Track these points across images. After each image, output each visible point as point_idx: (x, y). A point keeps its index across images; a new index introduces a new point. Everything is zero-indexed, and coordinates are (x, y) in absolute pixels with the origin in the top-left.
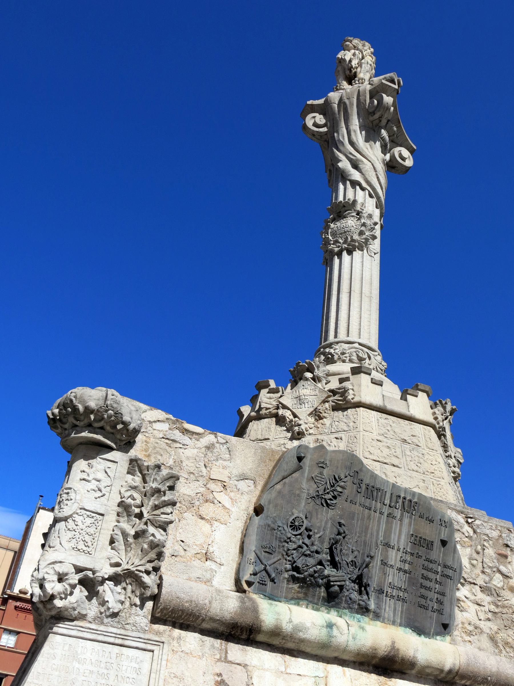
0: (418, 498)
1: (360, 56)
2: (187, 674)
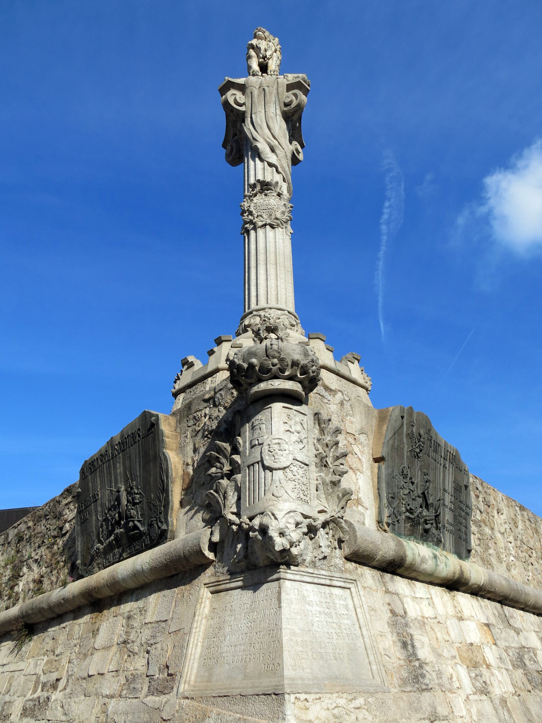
0: (456, 453)
1: (270, 46)
2: (376, 606)
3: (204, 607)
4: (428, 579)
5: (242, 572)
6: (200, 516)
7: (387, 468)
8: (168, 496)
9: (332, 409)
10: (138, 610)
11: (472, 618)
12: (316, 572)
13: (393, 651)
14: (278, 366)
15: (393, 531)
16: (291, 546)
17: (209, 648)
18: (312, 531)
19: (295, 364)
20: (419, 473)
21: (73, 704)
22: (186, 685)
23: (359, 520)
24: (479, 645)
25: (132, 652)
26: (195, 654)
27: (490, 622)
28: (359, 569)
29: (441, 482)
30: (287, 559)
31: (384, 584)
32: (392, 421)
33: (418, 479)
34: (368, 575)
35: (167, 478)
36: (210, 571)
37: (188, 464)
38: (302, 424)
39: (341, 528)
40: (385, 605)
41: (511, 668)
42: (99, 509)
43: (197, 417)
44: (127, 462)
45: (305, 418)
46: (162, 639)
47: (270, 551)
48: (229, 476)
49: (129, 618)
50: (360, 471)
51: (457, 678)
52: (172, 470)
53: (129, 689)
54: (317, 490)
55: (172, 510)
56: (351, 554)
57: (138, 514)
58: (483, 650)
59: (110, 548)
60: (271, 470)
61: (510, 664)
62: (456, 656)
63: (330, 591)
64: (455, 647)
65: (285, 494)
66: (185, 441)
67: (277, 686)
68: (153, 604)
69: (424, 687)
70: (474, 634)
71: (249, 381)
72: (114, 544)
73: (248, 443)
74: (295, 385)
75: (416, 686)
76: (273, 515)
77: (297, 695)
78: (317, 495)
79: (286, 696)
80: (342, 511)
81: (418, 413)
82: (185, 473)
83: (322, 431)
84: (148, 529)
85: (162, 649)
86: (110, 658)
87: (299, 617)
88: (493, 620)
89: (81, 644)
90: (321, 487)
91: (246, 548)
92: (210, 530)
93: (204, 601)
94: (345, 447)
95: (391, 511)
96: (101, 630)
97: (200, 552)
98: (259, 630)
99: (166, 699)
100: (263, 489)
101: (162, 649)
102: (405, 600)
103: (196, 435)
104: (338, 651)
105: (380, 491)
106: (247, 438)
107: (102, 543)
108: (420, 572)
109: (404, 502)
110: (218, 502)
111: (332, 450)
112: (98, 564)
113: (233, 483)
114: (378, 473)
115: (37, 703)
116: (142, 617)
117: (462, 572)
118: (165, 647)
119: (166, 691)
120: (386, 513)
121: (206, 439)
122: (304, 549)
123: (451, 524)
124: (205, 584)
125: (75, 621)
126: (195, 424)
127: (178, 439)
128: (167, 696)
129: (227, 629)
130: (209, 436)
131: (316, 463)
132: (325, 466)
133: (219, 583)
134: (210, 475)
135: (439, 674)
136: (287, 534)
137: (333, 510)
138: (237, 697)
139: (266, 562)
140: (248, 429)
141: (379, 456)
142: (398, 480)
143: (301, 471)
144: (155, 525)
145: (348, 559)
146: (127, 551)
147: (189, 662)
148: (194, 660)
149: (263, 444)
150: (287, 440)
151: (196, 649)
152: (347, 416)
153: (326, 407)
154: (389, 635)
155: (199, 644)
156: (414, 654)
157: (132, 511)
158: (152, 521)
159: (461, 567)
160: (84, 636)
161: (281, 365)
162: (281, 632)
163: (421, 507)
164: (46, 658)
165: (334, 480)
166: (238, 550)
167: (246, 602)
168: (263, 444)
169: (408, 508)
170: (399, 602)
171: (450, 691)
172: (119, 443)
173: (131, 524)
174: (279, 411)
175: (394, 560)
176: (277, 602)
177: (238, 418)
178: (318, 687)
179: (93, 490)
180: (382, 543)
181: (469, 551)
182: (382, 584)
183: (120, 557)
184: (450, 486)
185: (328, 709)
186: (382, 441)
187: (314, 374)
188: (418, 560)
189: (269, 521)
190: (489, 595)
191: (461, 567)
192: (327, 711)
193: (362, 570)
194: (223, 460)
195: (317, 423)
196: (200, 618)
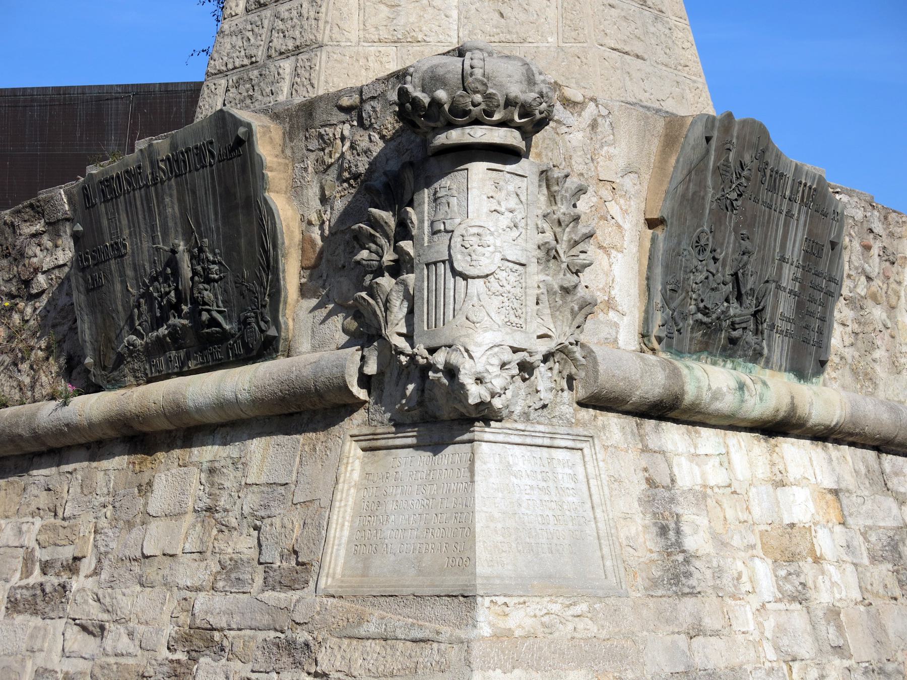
0: (818, 184)
2: (623, 475)
3: (352, 470)
4: (726, 423)
5: (413, 425)
6: (338, 321)
7: (668, 238)
8: (278, 280)
9: (575, 143)
10: (229, 461)
11: (805, 481)
12: (529, 428)
13: (641, 540)
14: (483, 106)
15: (669, 348)
16: (493, 397)
17: (362, 530)
18: (526, 368)
19: (509, 103)
20: (733, 237)
21: (120, 597)
22: (330, 580)
23: (608, 336)
24: (807, 526)
25: (227, 526)
26: (340, 538)
27: (843, 486)
28: (600, 418)
29: (778, 245)
30: (486, 414)
31: (642, 438)
32: (688, 149)
33: (728, 250)
34: (614, 425)
35: (275, 246)
36: (360, 416)
37: (310, 223)
38: (518, 195)
39: (574, 360)
40: (638, 471)
41: (866, 561)
42: (130, 273)
43: (326, 137)
44: (188, 199)
45: (523, 183)
46: (282, 511)
47: (460, 401)
48: (396, 270)
49: (212, 471)
50: (617, 250)
51: (750, 578)
52: (282, 233)
53: (228, 579)
54: (537, 303)
55: (285, 303)
56: (587, 398)
57: (217, 298)
58: (813, 533)
59: (160, 347)
60: (465, 277)
61: (865, 554)
62: (755, 545)
63: (550, 455)
64: (757, 531)
65: (486, 318)
66: (303, 178)
67: (467, 586)
68: (258, 456)
69: (687, 590)
70: (800, 506)
71: (432, 124)
72: (167, 343)
73: (426, 224)
74: (509, 134)
75: (674, 588)
76: (467, 351)
77: (494, 598)
78: (538, 310)
79: (479, 599)
80: (578, 331)
81: (744, 123)
82: (306, 241)
83: (552, 198)
84: (240, 329)
85: (283, 526)
86: (183, 531)
87: (500, 495)
88: (849, 481)
89: (117, 505)
90: (544, 298)
91: (421, 390)
92: (360, 353)
93: (351, 461)
94: (593, 209)
95: (668, 315)
96: (155, 487)
97: (344, 388)
98: (440, 511)
99: (298, 597)
100: (452, 307)
101: (283, 526)
102: (675, 461)
103: (325, 171)
104: (555, 541)
105: (651, 282)
106: (426, 214)
107: (141, 336)
108: (709, 414)
109: (694, 296)
110: (375, 313)
111: (568, 230)
112: (134, 371)
113: (401, 288)
114: (650, 250)
115: (39, 592)
116: (239, 474)
117: (793, 407)
118: (287, 525)
119: (296, 586)
120: (658, 318)
121: (345, 185)
122: (513, 397)
123: (788, 320)
124: (351, 436)
125: (95, 464)
126: (323, 150)
127: (290, 171)
128: (298, 592)
129: (391, 506)
130: (352, 181)
131: (538, 259)
132: (555, 258)
133: (375, 437)
134: (358, 263)
135: (718, 573)
136: (487, 381)
137: (561, 334)
138: (408, 598)
139: (453, 415)
140: (426, 200)
141: (655, 215)
142: (688, 257)
143: (513, 278)
144: (254, 325)
145: (582, 404)
146: (195, 358)
147: (333, 548)
148: (339, 545)
149: (453, 231)
150: (492, 229)
151: (342, 530)
152: (602, 147)
153: (564, 141)
154: (638, 518)
155: (346, 524)
156: (678, 544)
157: (205, 293)
158: (247, 317)
159: (792, 398)
160: (122, 492)
161: (487, 105)
162: (473, 517)
163: (727, 300)
164: (38, 522)
165: (566, 284)
166: (408, 393)
167: (421, 469)
168: (453, 231)
169: (701, 305)
170: (663, 466)
171: (733, 597)
172: (168, 158)
173: (205, 316)
174: (481, 176)
175: (661, 401)
176: (468, 474)
177: (409, 175)
178: (522, 589)
179: (111, 234)
180: (641, 377)
181: (823, 363)
182: (638, 439)
183: (181, 368)
184: (796, 249)
185: (535, 616)
186: (665, 187)
187: (543, 115)
188: (706, 397)
189: (461, 360)
190: (851, 439)
191: (792, 398)
192: (534, 619)
193: (605, 419)
194: (383, 241)
195: (544, 184)
196: (346, 486)
